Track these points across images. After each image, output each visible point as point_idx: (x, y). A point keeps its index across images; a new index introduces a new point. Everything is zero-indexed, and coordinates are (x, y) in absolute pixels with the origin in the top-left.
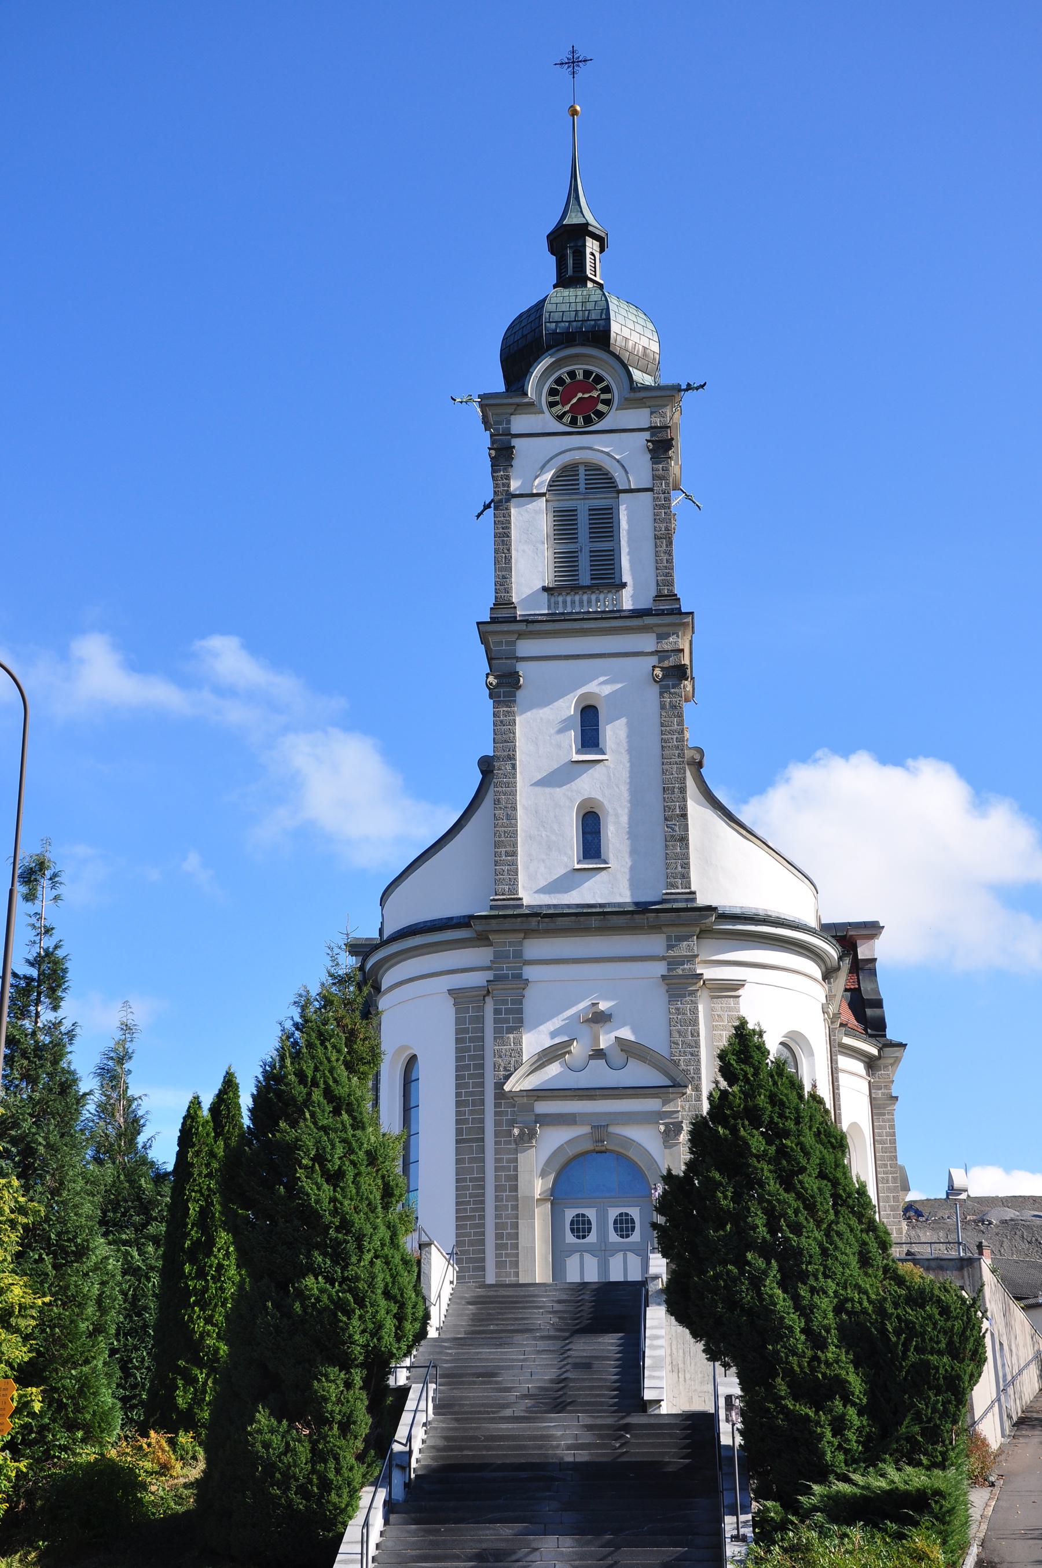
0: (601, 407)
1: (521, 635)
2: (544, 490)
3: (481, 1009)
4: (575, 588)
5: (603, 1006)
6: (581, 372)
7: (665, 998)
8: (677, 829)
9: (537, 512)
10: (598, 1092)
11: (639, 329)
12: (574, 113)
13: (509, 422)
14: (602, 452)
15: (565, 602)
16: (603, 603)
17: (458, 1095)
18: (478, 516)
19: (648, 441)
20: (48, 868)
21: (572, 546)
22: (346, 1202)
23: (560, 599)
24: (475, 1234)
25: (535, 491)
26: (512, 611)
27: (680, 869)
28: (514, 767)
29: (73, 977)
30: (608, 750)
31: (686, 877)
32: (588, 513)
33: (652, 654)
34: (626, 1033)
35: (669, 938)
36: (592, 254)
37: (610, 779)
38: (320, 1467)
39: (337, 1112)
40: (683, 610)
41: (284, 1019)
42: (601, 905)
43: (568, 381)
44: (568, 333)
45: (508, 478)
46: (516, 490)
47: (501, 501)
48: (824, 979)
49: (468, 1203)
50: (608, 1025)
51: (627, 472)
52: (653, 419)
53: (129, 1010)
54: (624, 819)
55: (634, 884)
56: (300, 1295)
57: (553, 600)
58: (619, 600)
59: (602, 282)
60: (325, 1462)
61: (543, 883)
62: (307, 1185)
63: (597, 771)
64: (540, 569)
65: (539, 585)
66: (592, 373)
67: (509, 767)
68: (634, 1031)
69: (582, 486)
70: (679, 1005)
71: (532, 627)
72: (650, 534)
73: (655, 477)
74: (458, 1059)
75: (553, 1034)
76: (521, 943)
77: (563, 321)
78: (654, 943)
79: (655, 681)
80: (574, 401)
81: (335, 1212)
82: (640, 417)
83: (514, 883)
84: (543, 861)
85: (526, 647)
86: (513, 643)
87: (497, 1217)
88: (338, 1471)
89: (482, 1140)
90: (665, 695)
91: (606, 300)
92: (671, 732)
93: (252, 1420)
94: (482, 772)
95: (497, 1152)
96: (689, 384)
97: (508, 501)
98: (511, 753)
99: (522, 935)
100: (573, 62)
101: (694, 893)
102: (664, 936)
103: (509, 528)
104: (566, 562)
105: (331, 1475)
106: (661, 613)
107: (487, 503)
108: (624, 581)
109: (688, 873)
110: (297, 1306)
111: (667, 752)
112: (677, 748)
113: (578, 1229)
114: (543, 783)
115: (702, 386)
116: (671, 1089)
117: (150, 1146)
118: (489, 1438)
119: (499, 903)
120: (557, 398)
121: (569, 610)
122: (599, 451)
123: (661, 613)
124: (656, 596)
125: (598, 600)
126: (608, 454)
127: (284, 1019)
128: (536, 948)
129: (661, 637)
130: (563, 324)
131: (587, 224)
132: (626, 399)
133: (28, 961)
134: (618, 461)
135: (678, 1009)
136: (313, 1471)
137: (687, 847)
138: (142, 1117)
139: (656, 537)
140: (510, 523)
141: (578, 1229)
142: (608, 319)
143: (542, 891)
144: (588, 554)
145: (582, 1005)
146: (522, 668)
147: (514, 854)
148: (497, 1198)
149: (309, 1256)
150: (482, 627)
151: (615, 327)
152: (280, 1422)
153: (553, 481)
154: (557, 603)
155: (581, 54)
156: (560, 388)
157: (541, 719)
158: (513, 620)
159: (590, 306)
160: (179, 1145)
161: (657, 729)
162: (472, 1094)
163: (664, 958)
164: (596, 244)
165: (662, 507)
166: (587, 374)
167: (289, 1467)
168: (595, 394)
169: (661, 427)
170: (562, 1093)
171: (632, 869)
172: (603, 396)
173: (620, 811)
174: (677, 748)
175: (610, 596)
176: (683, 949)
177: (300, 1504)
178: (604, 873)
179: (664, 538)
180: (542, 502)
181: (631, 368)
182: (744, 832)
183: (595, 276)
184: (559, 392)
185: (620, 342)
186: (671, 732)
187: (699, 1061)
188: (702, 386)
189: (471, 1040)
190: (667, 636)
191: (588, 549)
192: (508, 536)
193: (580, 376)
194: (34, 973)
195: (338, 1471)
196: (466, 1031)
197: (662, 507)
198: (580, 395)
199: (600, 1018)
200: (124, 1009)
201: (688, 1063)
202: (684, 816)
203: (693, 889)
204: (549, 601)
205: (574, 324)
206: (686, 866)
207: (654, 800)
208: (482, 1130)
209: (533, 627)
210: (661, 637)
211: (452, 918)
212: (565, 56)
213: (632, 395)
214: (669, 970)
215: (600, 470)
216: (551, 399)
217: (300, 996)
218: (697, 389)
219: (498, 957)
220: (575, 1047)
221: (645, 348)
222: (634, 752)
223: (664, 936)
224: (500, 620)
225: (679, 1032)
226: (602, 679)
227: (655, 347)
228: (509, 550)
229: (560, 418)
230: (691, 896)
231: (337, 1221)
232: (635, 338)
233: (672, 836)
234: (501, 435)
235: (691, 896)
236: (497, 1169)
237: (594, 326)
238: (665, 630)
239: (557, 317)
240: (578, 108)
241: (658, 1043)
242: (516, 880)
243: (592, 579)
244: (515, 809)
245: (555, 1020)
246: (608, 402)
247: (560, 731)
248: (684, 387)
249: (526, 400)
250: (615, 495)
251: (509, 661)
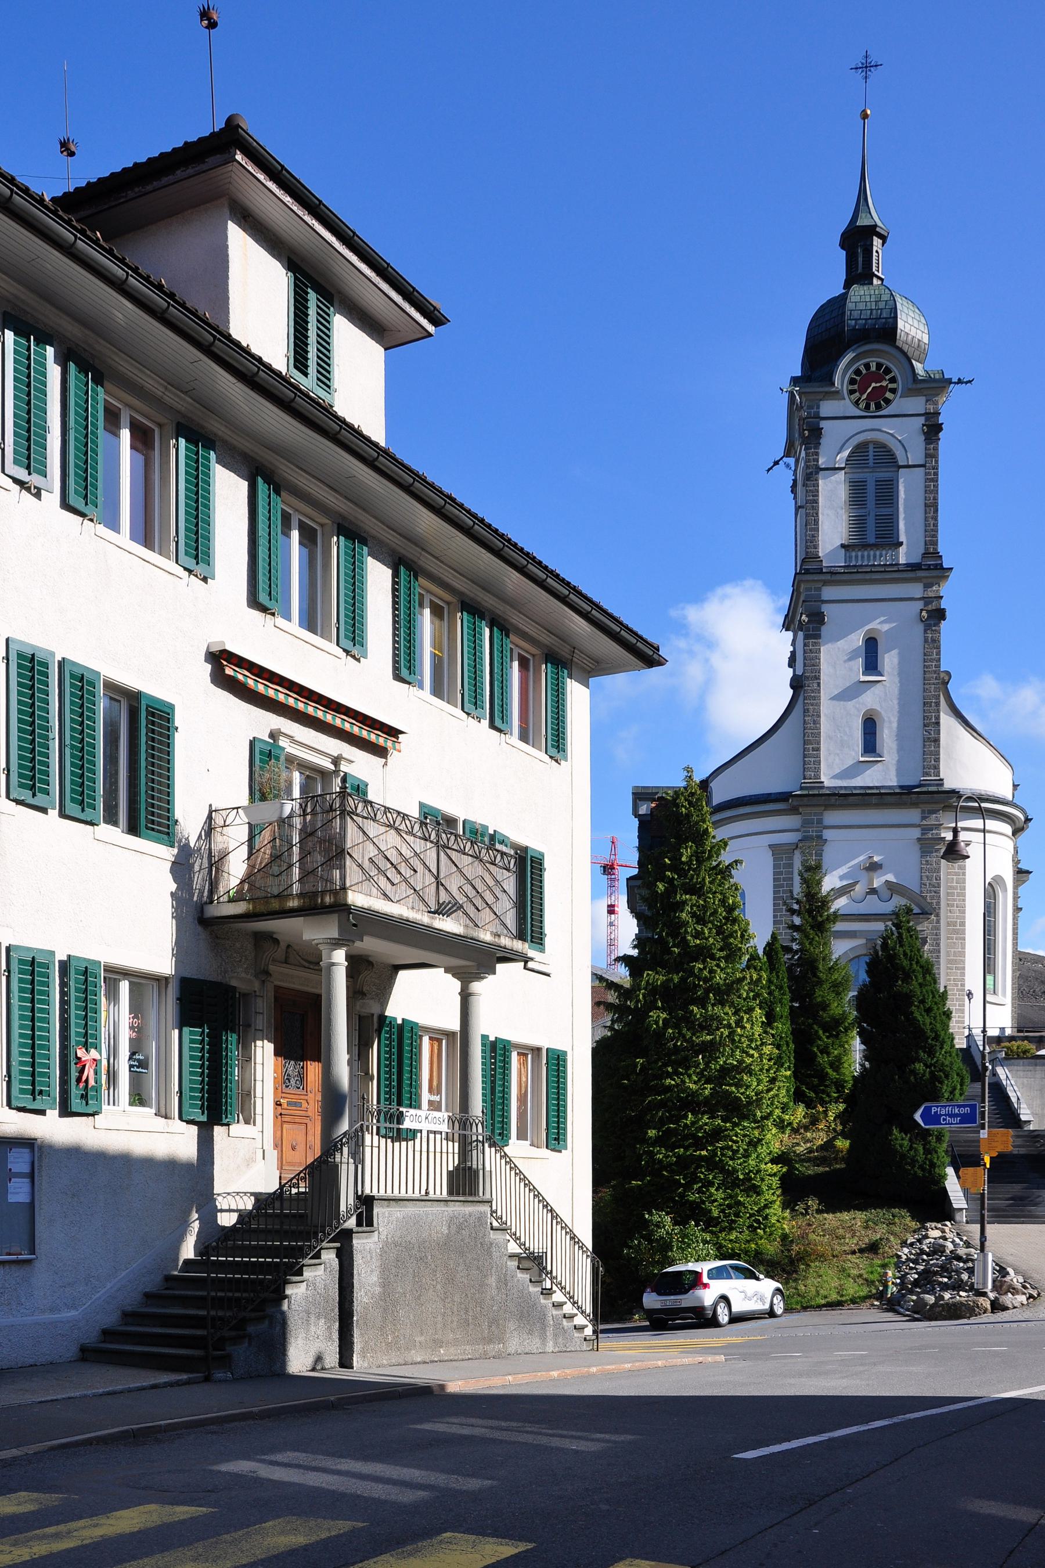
0: (888, 395)
1: (826, 583)
2: (843, 465)
3: (791, 858)
4: (865, 546)
5: (876, 859)
6: (874, 364)
7: (919, 854)
8: (932, 733)
9: (838, 483)
10: (873, 917)
11: (916, 324)
12: (865, 116)
13: (818, 407)
14: (888, 433)
15: (857, 557)
16: (884, 558)
17: (775, 916)
19: (923, 425)
21: (864, 510)
22: (938, 1025)
23: (854, 554)
25: (837, 466)
26: (819, 563)
27: (933, 762)
28: (819, 684)
30: (885, 673)
31: (937, 768)
32: (874, 483)
33: (920, 599)
34: (891, 878)
35: (923, 812)
36: (877, 252)
37: (886, 695)
38: (929, 1156)
40: (945, 566)
42: (877, 788)
43: (864, 372)
44: (865, 329)
45: (817, 454)
46: (822, 464)
47: (811, 473)
48: (1014, 834)
50: (879, 871)
51: (906, 452)
52: (928, 406)
54: (895, 725)
55: (899, 772)
56: (913, 1072)
58: (898, 558)
59: (883, 277)
60: (931, 1154)
61: (837, 771)
62: (917, 1015)
63: (877, 689)
64: (840, 530)
65: (839, 544)
67: (815, 685)
68: (896, 877)
70: (928, 859)
72: (921, 502)
73: (927, 456)
75: (841, 878)
76: (822, 814)
77: (860, 319)
78: (913, 815)
79: (922, 621)
80: (869, 390)
81: (932, 1030)
82: (916, 404)
83: (818, 770)
84: (838, 755)
85: (829, 592)
86: (819, 589)
88: (938, 1158)
90: (928, 632)
91: (894, 300)
92: (931, 660)
93: (891, 1134)
96: (959, 379)
97: (817, 473)
98: (817, 674)
99: (823, 808)
100: (866, 67)
101: (942, 780)
102: (919, 810)
103: (818, 496)
104: (858, 524)
105: (935, 1161)
106: (929, 568)
109: (939, 765)
110: (912, 1078)
111: (927, 676)
112: (935, 672)
114: (837, 698)
115: (970, 382)
116: (921, 916)
118: (965, 1141)
119: (808, 785)
120: (856, 387)
121: (859, 563)
122: (885, 432)
123: (929, 568)
124: (924, 554)
125: (881, 556)
126: (891, 435)
128: (832, 817)
129: (927, 586)
130: (860, 321)
131: (876, 226)
132: (909, 389)
134: (900, 441)
135: (927, 861)
136: (926, 1158)
137: (939, 747)
139: (926, 505)
140: (818, 492)
142: (896, 317)
143: (835, 777)
145: (861, 858)
146: (826, 609)
147: (818, 749)
149: (917, 1053)
151: (900, 324)
152: (906, 1135)
154: (851, 557)
155: (874, 59)
156: (858, 378)
157: (839, 648)
158: (820, 571)
159: (882, 305)
161: (921, 657)
163: (919, 826)
164: (880, 241)
165: (932, 480)
166: (879, 366)
167: (914, 1157)
168: (884, 384)
169: (933, 413)
170: (849, 917)
171: (898, 761)
172: (890, 386)
173: (892, 719)
174: (935, 672)
175: (890, 552)
176: (932, 820)
177: (920, 1173)
178: (879, 764)
179: (931, 507)
180: (841, 476)
181: (914, 362)
182: (975, 735)
183: (878, 271)
184: (860, 381)
185: (903, 337)
186: (931, 660)
187: (940, 897)
190: (931, 585)
192: (816, 502)
193: (873, 368)
195: (938, 1158)
196: (781, 873)
197: (932, 480)
198: (873, 385)
199: (874, 867)
201: (932, 898)
202: (938, 724)
203: (941, 777)
205: (870, 321)
206: (938, 760)
207: (917, 710)
209: (834, 577)
210: (927, 586)
212: (859, 60)
213: (914, 386)
214: (923, 834)
215: (885, 447)
216: (850, 387)
218: (966, 383)
219: (806, 823)
220: (857, 888)
221: (919, 340)
222: (903, 673)
223: (919, 810)
224: (811, 571)
225: (927, 877)
226: (882, 619)
227: (926, 339)
228: (817, 514)
229: (857, 403)
230: (940, 782)
231: (933, 1035)
232: (913, 332)
233: (929, 738)
235: (940, 782)
237: (885, 323)
238: (930, 580)
239: (856, 314)
240: (869, 112)
241: (913, 884)
242: (819, 768)
243: (876, 538)
244: (819, 716)
245: (844, 867)
246: (893, 391)
247: (850, 659)
248: (955, 380)
249: (834, 389)
250: (896, 469)
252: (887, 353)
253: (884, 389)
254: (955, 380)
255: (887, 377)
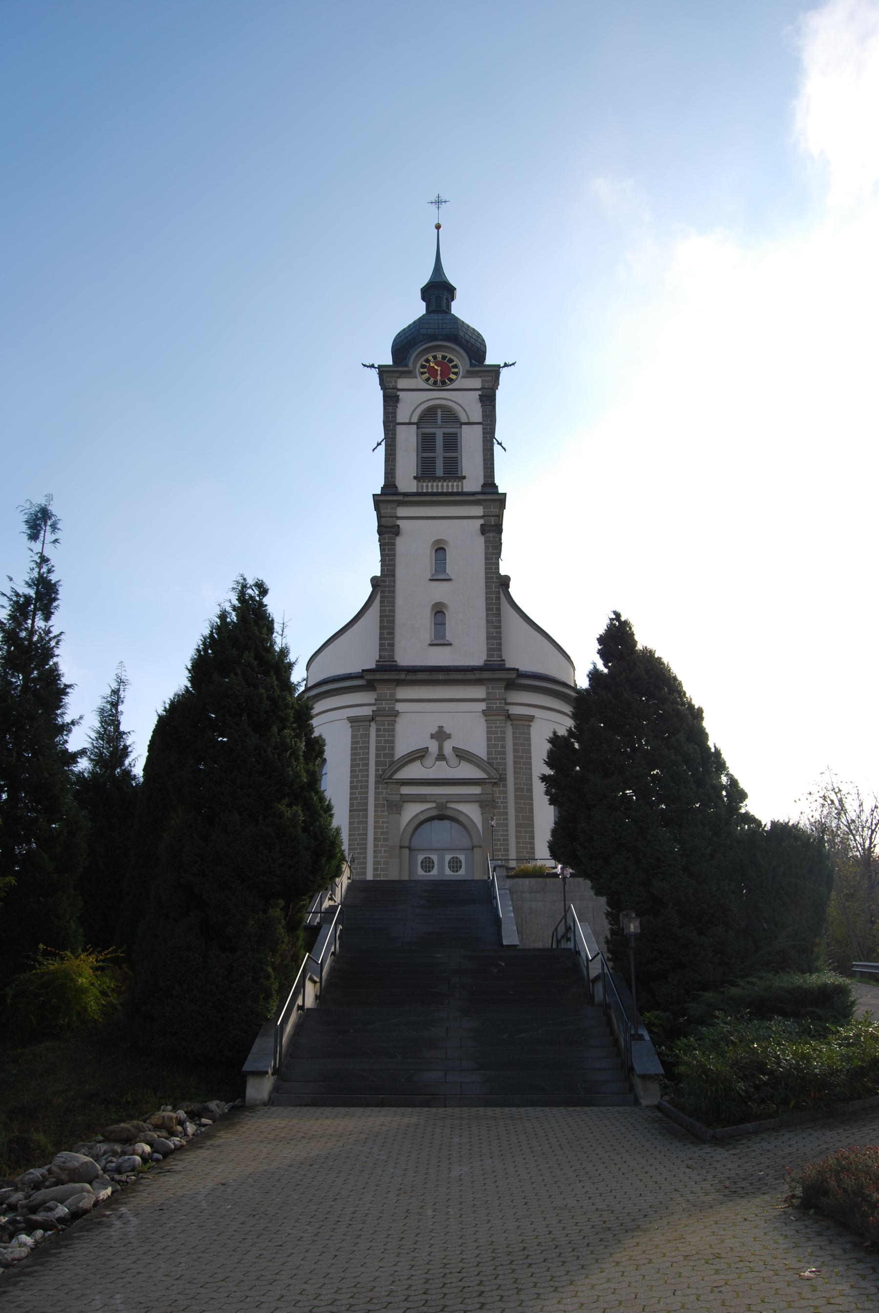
6: (440, 356)
13: (396, 382)
17: (351, 782)
18: (373, 450)
20: (50, 518)
24: (360, 868)
29: (63, 593)
32: (442, 435)
39: (266, 674)
41: (223, 601)
49: (356, 849)
53: (123, 669)
57: (420, 484)
58: (365, 873)
66: (447, 357)
69: (439, 421)
71: (406, 499)
74: (352, 760)
87: (375, 857)
89: (366, 810)
94: (373, 586)
95: (376, 817)
96: (505, 363)
107: (379, 442)
108: (464, 475)
113: (426, 866)
115: (513, 364)
116: (487, 781)
117: (134, 765)
127: (223, 601)
128: (403, 693)
133: (27, 583)
138: (130, 746)
141: (426, 866)
144: (442, 459)
148: (375, 846)
150: (376, 498)
153: (422, 417)
160: (148, 751)
162: (360, 781)
166: (444, 357)
188: (513, 364)
189: (361, 748)
191: (442, 457)
194: (32, 592)
196: (358, 743)
200: (120, 667)
204: (417, 485)
208: (366, 804)
209: (409, 500)
211: (351, 674)
212: (434, 199)
213: (471, 369)
216: (422, 370)
217: (238, 583)
218: (510, 365)
234: (391, 389)
236: (375, 828)
243: (444, 474)
246: (455, 374)
248: (502, 365)
250: (459, 426)
251: (391, 519)
252: (459, 353)
253: (435, 376)
254: (502, 365)
255: (427, 364)
